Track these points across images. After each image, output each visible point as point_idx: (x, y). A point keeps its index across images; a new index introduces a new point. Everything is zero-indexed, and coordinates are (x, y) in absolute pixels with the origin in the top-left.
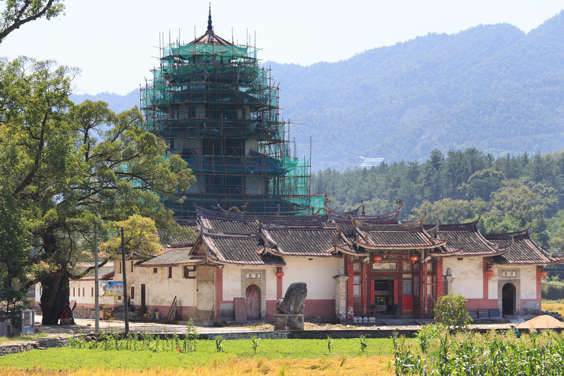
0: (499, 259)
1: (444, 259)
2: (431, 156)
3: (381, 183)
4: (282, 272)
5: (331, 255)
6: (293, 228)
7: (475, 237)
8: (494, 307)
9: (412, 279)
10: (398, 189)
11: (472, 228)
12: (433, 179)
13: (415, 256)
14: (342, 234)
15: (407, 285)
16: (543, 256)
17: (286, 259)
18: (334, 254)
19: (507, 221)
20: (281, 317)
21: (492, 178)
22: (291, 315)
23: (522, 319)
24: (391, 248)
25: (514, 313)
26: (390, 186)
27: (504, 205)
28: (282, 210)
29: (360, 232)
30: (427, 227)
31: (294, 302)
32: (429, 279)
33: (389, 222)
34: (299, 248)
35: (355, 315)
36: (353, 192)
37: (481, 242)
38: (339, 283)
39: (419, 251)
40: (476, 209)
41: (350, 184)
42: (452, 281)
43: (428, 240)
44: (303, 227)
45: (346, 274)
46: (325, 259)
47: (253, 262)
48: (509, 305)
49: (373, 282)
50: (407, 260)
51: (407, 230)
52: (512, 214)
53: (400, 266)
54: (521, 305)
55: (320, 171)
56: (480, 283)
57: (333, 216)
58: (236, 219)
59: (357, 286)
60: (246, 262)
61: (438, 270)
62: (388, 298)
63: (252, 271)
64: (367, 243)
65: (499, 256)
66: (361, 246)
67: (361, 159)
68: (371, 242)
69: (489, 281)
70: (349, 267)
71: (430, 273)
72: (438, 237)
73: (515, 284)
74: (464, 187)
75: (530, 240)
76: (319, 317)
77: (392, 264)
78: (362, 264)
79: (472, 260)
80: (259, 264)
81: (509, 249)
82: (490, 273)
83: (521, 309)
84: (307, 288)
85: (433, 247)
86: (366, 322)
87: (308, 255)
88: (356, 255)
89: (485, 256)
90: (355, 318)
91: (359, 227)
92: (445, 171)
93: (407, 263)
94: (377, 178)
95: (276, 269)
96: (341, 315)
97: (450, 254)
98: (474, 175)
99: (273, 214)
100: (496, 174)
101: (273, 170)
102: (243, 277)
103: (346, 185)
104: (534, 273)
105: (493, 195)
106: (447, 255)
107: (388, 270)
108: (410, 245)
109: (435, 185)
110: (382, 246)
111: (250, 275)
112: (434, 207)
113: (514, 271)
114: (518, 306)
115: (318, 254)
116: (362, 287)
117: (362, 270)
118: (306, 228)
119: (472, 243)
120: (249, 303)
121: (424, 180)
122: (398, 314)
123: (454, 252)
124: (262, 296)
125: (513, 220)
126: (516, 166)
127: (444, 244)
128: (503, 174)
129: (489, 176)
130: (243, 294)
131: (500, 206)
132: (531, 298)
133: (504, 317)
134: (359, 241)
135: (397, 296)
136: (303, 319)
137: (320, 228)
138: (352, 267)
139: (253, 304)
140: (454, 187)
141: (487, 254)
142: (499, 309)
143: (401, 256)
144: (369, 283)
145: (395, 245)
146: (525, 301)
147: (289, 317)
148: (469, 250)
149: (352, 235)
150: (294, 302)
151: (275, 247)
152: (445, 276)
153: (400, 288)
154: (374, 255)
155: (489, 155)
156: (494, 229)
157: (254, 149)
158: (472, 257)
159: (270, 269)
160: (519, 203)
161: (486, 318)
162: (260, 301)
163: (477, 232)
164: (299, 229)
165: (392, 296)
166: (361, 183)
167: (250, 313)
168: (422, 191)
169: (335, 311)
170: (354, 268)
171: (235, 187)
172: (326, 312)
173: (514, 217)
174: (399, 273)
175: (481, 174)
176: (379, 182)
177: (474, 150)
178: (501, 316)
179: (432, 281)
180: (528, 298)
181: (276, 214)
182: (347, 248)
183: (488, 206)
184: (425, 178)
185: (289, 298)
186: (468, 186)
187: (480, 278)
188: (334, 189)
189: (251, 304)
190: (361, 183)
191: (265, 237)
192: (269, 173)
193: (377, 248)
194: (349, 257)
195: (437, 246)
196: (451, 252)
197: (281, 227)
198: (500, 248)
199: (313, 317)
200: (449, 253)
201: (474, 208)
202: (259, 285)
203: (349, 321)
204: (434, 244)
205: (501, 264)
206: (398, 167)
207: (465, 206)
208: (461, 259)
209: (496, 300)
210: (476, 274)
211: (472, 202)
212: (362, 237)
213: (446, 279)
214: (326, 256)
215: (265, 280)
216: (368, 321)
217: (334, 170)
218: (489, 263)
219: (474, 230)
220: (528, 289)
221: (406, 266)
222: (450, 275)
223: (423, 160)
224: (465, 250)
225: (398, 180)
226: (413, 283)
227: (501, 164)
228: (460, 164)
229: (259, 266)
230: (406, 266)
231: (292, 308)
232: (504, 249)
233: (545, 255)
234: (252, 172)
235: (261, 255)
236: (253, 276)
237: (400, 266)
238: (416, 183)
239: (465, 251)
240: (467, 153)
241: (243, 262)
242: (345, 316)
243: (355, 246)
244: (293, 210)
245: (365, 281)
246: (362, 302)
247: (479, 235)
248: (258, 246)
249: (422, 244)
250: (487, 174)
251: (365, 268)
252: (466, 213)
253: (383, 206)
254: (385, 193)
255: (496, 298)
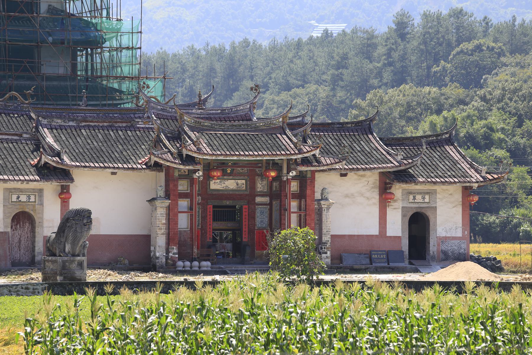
0: (403, 176)
1: (317, 175)
2: (394, 22)
3: (321, 61)
4: (68, 192)
5: (144, 167)
6: (89, 126)
7: (369, 142)
8: (396, 248)
9: (271, 204)
10: (344, 71)
11: (363, 128)
12: (396, 55)
13: (273, 170)
14: (163, 136)
15: (262, 213)
16: (472, 172)
17: (75, 173)
18: (148, 166)
19: (495, 119)
20: (53, 262)
21: (487, 54)
22: (66, 258)
23: (438, 267)
24: (235, 158)
25: (427, 257)
26: (333, 66)
27: (491, 94)
28: (89, 99)
29: (191, 133)
30: (293, 127)
31: (71, 238)
32: (294, 205)
33: (240, 118)
34: (98, 157)
35: (180, 259)
36: (279, 75)
37: (377, 150)
38: (156, 209)
39: (279, 162)
40: (450, 101)
41: (276, 62)
42: (328, 208)
43: (292, 146)
44: (105, 124)
45: (168, 196)
46: (135, 173)
47: (22, 178)
48: (420, 244)
49: (210, 208)
50: (263, 176)
51: (262, 130)
52: (503, 109)
53: (252, 185)
54: (439, 245)
55: (233, 43)
56: (376, 210)
57: (153, 108)
58: (16, 110)
59: (295, 215)
60: (11, 177)
61: (308, 192)
62: (237, 232)
63: (21, 191)
64: (199, 149)
65: (405, 171)
66: (190, 153)
67: (311, 26)
68: (204, 148)
69: (388, 209)
70: (171, 186)
71: (295, 196)
72: (309, 142)
73: (429, 214)
74: (444, 68)
75: (455, 148)
76: (126, 262)
77: (239, 181)
78: (192, 182)
79: (362, 176)
80: (31, 181)
81: (418, 161)
82: (389, 196)
83: (438, 251)
84: (92, 217)
85: (300, 156)
86: (197, 269)
87: (109, 168)
88: (182, 167)
89: (382, 170)
90: (180, 263)
91: (188, 126)
92: (415, 43)
93: (262, 180)
94: (316, 53)
95: (59, 188)
96: (157, 258)
97: (325, 168)
98: (458, 49)
99: (75, 105)
100: (493, 48)
101: (83, 37)
102: (6, 199)
103: (271, 64)
104: (458, 196)
105: (485, 80)
106: (322, 168)
107: (233, 190)
108: (264, 153)
109: (398, 65)
110: (220, 155)
111: (18, 198)
112: (386, 98)
113: (428, 193)
114: (433, 247)
115: (125, 166)
116: (192, 216)
117: (192, 190)
118: (111, 126)
119: (363, 151)
120: (16, 240)
121: (384, 57)
122: (247, 257)
123: (332, 164)
124: (37, 230)
125: (504, 117)
126: (526, 35)
127: (317, 152)
128: (504, 48)
129: (482, 50)
130: (6, 227)
131: (485, 96)
132: (454, 235)
133: (410, 263)
134: (186, 147)
135: (247, 229)
136: (85, 264)
137: (132, 126)
138: (176, 186)
139: (23, 242)
140: (429, 68)
141: (384, 168)
142: (403, 252)
143: (253, 170)
144: (204, 210)
145: (242, 153)
146: (445, 239)
147: (64, 262)
148: (357, 162)
149: (177, 137)
150: (71, 238)
151: (58, 155)
152: (319, 200)
153: (252, 216)
154: (211, 167)
155: (486, 18)
156: (471, 130)
157: (55, 5)
158: (361, 173)
159: (50, 188)
160: (515, 91)
161: (383, 265)
162: (34, 237)
163: (372, 134)
164: (98, 128)
165: (240, 230)
166: (292, 61)
167: (17, 256)
168: (379, 75)
169: (150, 252)
170: (180, 188)
171: (22, 62)
172: (134, 255)
173: (506, 112)
174: (250, 195)
175: (471, 48)
176: (319, 59)
177: (461, 10)
178: (407, 261)
179: (300, 208)
180: (448, 235)
181: (79, 105)
182: (169, 157)
183: (468, 96)
184: (385, 55)
185: (64, 232)
186: (449, 65)
187: (374, 204)
188: (252, 69)
189: (20, 241)
190: (292, 61)
191: (44, 139)
192: (77, 43)
193: (214, 158)
194: (171, 171)
195: (306, 155)
196: (328, 165)
197: (71, 123)
198: (405, 159)
199: (117, 262)
200: (324, 165)
201: (446, 99)
202: (32, 212)
203: (170, 268)
204: (300, 152)
205: (406, 182)
206: (347, 38)
207: (434, 96)
208: (345, 175)
209: (399, 237)
210: (368, 198)
211: (444, 90)
212: (192, 140)
213: (319, 204)
214: (137, 169)
215: (42, 204)
216: (199, 267)
217: (254, 41)
218: (388, 181)
219: (367, 131)
220: (448, 220)
221: (261, 186)
222: (327, 199)
223: (383, 26)
224: (351, 161)
225: (345, 57)
226: (271, 210)
227: (501, 32)
228: (438, 32)
229: (30, 183)
230: (261, 186)
231: (68, 248)
232: (410, 161)
233: (476, 170)
234: (50, 39)
235: (36, 166)
236: (23, 198)
237: (252, 185)
238: (371, 62)
239: (351, 163)
240: (450, 16)
241: (6, 177)
242: (164, 260)
243: (180, 155)
244: (114, 99)
245: (197, 209)
246: (192, 238)
247: (375, 138)
248: (32, 153)
249: (283, 152)
250: (479, 48)
251: (196, 187)
252: (434, 107)
253: (321, 95)
254: (324, 77)
255: (400, 234)
